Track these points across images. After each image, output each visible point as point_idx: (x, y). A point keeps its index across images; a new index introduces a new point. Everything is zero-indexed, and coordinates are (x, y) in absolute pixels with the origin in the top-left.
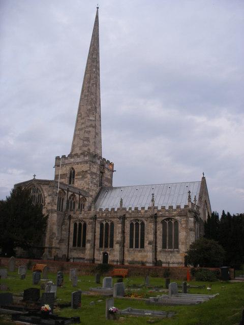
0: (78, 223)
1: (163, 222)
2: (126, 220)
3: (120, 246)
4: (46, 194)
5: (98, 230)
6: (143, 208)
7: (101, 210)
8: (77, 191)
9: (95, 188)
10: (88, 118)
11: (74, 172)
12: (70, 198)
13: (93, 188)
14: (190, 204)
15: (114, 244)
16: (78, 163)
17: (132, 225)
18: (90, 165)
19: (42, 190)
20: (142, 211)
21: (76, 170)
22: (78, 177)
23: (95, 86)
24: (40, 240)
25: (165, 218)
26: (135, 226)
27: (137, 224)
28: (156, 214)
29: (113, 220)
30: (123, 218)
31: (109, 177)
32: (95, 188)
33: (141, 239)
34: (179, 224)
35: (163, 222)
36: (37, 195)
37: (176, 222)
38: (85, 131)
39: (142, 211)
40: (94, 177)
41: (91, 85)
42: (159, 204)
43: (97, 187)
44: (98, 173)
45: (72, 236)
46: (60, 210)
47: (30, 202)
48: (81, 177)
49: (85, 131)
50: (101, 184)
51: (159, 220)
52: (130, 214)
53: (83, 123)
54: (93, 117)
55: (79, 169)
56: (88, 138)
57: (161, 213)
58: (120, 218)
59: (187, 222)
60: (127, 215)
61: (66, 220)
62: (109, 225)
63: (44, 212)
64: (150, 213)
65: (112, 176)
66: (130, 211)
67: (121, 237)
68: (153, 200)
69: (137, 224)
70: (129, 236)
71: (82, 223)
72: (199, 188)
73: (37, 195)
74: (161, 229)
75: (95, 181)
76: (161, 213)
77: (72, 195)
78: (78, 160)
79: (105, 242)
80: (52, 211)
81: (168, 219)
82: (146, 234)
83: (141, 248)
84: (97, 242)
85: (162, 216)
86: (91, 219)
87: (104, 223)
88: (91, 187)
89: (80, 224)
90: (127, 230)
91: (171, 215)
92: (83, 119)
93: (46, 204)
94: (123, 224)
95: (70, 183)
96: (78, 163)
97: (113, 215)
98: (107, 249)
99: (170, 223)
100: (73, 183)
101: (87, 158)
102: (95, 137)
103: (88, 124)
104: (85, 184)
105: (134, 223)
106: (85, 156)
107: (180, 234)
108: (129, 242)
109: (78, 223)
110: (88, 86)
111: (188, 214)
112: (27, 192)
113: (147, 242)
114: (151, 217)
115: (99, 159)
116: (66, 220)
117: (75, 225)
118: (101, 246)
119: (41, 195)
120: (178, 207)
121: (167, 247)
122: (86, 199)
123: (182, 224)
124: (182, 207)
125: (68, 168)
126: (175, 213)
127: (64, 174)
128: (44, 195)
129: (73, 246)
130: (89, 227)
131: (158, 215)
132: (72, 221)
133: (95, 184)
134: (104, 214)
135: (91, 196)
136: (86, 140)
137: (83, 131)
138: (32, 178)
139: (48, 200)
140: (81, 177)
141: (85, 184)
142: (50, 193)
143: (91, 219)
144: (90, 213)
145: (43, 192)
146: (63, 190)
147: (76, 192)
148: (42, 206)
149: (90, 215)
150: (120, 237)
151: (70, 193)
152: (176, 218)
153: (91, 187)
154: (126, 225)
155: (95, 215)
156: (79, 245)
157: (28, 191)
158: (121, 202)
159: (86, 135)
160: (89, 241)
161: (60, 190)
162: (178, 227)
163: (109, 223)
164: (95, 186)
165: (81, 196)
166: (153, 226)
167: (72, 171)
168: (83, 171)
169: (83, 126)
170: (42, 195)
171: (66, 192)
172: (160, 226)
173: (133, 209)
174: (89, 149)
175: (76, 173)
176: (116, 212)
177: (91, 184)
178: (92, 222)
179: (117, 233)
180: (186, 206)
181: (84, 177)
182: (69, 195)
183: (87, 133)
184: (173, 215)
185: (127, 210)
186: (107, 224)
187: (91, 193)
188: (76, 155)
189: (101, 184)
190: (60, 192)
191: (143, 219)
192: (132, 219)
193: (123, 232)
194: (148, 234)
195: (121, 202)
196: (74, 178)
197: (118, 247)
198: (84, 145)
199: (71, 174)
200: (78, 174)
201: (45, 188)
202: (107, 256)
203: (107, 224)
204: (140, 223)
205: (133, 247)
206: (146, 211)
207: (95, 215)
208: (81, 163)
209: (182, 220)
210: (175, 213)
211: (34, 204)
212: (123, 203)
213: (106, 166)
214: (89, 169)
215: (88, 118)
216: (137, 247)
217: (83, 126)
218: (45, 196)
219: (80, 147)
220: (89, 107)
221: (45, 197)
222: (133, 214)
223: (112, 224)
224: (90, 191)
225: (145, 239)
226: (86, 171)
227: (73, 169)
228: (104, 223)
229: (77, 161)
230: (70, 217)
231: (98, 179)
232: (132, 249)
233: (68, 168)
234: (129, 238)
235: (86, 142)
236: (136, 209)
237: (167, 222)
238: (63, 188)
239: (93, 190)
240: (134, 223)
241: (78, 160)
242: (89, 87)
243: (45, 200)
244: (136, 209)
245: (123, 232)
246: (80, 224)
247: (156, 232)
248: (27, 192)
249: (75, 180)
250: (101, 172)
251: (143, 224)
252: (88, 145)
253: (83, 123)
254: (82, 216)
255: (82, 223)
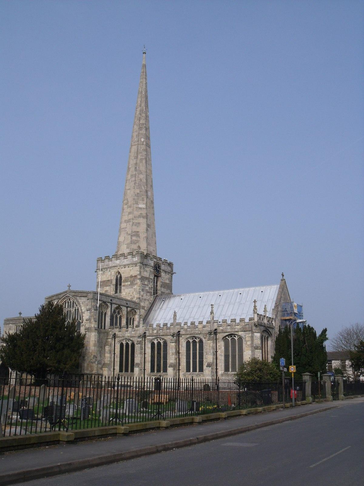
0: (124, 343)
1: (224, 338)
2: (181, 338)
3: (174, 369)
4: (84, 309)
5: (148, 351)
6: (201, 323)
7: (158, 325)
8: (124, 303)
9: (148, 297)
10: (137, 206)
11: (121, 277)
12: (115, 312)
13: (145, 297)
14: (256, 315)
15: (168, 368)
16: (125, 266)
17: (188, 343)
18: (141, 268)
19: (79, 304)
20: (200, 326)
21: (122, 275)
22: (126, 284)
23: (144, 161)
24: (78, 366)
25: (227, 334)
26: (191, 344)
27: (194, 342)
28: (216, 330)
29: (165, 338)
30: (178, 334)
31: (167, 282)
32: (148, 297)
33: (164, 362)
34: (244, 340)
35: (224, 338)
36: (73, 310)
37: (240, 339)
38: (133, 223)
39: (200, 326)
40: (146, 283)
41: (138, 162)
42: (220, 317)
43: (151, 295)
44: (152, 277)
45: (117, 360)
46: (101, 328)
47: (64, 320)
48: (129, 283)
49: (133, 223)
50: (155, 292)
51: (220, 336)
52: (186, 330)
53: (130, 213)
54: (144, 204)
55: (126, 273)
56: (138, 232)
57: (221, 328)
58: (173, 336)
59: (252, 337)
60: (182, 332)
61: (109, 340)
62: (162, 344)
63: (82, 330)
64: (208, 329)
65: (171, 280)
66: (186, 327)
67: (176, 359)
68: (212, 313)
69: (194, 342)
70: (185, 357)
71: (130, 343)
72: (277, 292)
73: (73, 310)
74: (223, 348)
75: (147, 288)
76: (221, 328)
77: (117, 308)
78: (126, 262)
79: (158, 365)
80: (88, 329)
81: (231, 335)
82: (205, 354)
83: (164, 372)
84: (148, 366)
85: (223, 332)
86: (139, 337)
87: (156, 342)
88: (142, 296)
89: (127, 344)
90: (183, 350)
91: (233, 330)
92: (130, 207)
93: (85, 321)
94: (178, 342)
95: (116, 292)
96: (125, 266)
97: (166, 331)
98: (159, 374)
99: (233, 340)
100: (120, 292)
101: (136, 259)
102: (147, 230)
103: (137, 213)
104: (134, 293)
105: (191, 341)
106: (133, 256)
107: (244, 353)
108: (185, 364)
109: (124, 343)
110: (135, 162)
111: (254, 328)
112: (60, 309)
113: (206, 364)
114: (210, 333)
115: (151, 259)
116: (109, 340)
117: (122, 345)
118: (152, 370)
119: (78, 309)
120: (242, 320)
121: (230, 370)
122: (135, 312)
123: (246, 341)
124: (247, 320)
125: (113, 272)
126: (239, 327)
127: (108, 281)
128: (82, 310)
129: (120, 372)
130: (137, 347)
131: (218, 331)
132: (117, 340)
133: (148, 292)
134: (155, 332)
135: (143, 308)
136: (134, 235)
137: (131, 223)
138: (66, 289)
139: (86, 316)
140: (129, 283)
141: (134, 293)
142: (88, 307)
143: (139, 337)
144: (137, 331)
145: (80, 306)
146: (104, 302)
147: (122, 304)
148: (79, 324)
149: (138, 332)
150: (174, 359)
151: (114, 306)
152: (240, 333)
153: (142, 296)
154: (180, 343)
155: (145, 333)
156: (127, 370)
157: (61, 306)
158: (175, 315)
159: (135, 229)
160: (138, 365)
161: (101, 302)
162: (242, 344)
163: (162, 342)
164: (148, 294)
165: (129, 309)
166: (211, 345)
167: (119, 277)
168: (131, 277)
169: (131, 216)
170: (79, 309)
171: (109, 304)
172: (221, 345)
173: (189, 324)
174: (139, 247)
175: (123, 279)
176: (169, 329)
177: (142, 293)
178: (141, 341)
179: (171, 354)
180: (251, 319)
181: (132, 284)
182: (113, 309)
183: (135, 225)
184: (236, 330)
185: (182, 325)
186: (159, 343)
187: (142, 304)
188: (123, 255)
189: (155, 292)
190: (100, 305)
191: (201, 337)
192: (188, 336)
193: (178, 353)
194: (207, 354)
195: (175, 315)
196: (120, 285)
197: (172, 371)
198: (132, 242)
199: (117, 280)
200: (126, 281)
201: (82, 300)
202: (160, 383)
203: (159, 343)
204: (197, 340)
205: (190, 371)
206: (204, 327)
207: (145, 333)
208: (128, 265)
209: (246, 336)
210: (239, 327)
211: (69, 320)
212: (177, 318)
213: (163, 267)
214: (139, 273)
215: (137, 206)
216: (195, 370)
217: (131, 216)
218: (83, 311)
219: (127, 244)
220: (138, 191)
221: (82, 312)
222: (188, 330)
223: (165, 343)
224: (140, 301)
225: (204, 360)
226: (136, 276)
227: (119, 273)
228: (156, 342)
229: (124, 264)
230: (115, 336)
231: (151, 285)
232: (189, 373)
233: (113, 273)
234: (185, 360)
235: (134, 238)
236: (193, 323)
237: (230, 339)
238: (105, 300)
239: (145, 300)
240: (191, 341)
241: (126, 262)
242: (136, 164)
243: (82, 317)
244: (193, 323)
245: (178, 353)
246: (127, 344)
247: (216, 352)
248: (60, 309)
249: (123, 288)
250: (155, 276)
251: (201, 342)
252: (138, 241)
253: (130, 213)
254: (129, 335)
255: (130, 343)
